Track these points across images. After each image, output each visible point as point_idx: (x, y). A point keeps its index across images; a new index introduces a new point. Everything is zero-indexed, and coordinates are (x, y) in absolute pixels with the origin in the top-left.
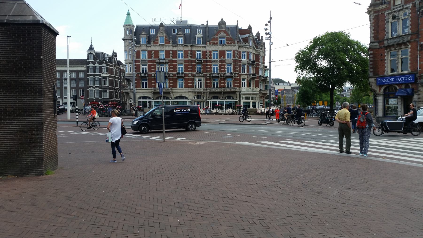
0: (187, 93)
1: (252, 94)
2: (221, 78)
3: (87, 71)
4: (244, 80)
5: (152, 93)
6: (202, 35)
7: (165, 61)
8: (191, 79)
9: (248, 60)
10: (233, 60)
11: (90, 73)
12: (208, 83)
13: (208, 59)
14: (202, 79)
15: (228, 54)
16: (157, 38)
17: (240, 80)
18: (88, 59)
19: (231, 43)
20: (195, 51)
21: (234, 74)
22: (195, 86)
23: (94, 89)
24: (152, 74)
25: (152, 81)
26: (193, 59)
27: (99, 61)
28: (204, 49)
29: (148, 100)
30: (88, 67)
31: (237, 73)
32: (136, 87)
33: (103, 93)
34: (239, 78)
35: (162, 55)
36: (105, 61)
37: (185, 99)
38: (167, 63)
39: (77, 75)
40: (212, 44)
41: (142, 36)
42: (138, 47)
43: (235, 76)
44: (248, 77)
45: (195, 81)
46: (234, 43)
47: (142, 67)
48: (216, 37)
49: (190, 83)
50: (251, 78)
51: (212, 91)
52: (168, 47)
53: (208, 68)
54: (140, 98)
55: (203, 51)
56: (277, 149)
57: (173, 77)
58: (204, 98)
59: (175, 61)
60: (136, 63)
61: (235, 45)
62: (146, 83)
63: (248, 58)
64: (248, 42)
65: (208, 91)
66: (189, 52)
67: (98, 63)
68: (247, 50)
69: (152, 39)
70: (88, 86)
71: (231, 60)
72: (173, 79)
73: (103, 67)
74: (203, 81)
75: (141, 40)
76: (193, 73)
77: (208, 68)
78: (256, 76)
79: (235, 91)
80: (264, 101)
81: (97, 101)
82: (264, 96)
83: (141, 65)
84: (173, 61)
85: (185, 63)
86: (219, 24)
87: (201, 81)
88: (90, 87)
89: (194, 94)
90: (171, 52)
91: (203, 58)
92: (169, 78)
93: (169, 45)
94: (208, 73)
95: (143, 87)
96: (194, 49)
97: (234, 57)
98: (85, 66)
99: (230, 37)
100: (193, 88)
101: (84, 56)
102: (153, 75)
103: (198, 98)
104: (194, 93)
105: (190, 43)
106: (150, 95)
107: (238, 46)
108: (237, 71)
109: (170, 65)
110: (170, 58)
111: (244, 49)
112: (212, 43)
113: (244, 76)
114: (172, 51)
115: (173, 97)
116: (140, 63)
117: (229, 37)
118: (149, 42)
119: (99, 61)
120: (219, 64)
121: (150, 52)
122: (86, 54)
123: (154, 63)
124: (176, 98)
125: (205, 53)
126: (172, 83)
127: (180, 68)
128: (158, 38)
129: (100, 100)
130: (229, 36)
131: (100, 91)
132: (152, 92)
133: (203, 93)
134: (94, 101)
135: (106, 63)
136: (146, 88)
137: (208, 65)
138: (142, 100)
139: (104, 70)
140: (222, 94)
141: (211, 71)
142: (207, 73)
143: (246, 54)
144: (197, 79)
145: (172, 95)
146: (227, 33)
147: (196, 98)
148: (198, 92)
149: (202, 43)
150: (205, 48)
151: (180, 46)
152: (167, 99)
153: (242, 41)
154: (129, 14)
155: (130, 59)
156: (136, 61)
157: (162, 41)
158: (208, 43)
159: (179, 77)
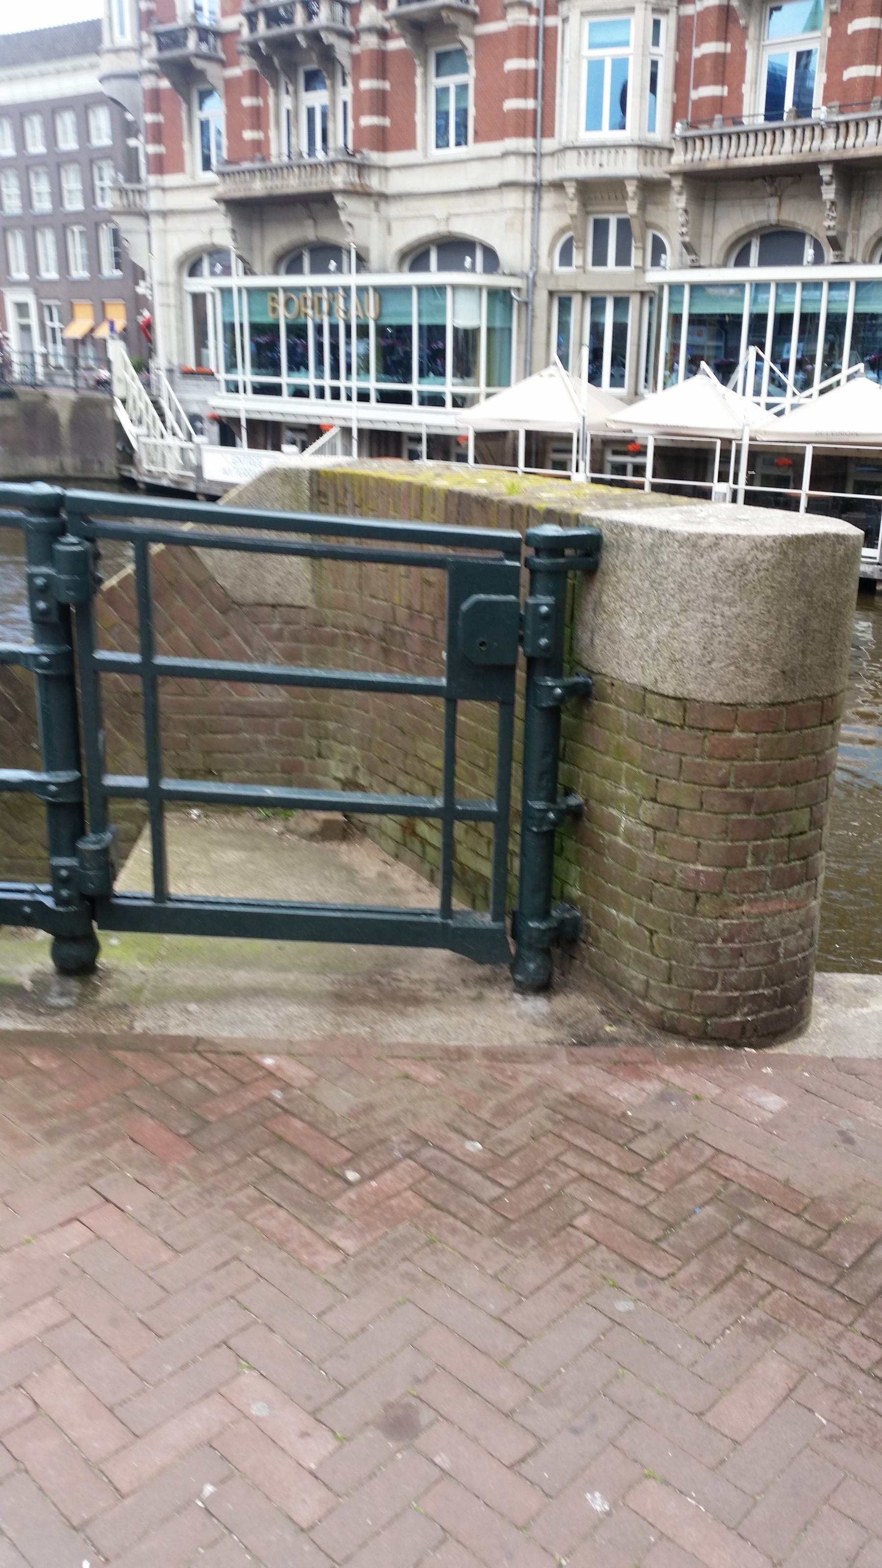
0: (493, 201)
56: (357, 919)
87: (626, 44)
95: (442, 141)
100: (548, 144)
103: (600, 259)
136: (462, 152)
140: (829, 193)
147: (582, 257)
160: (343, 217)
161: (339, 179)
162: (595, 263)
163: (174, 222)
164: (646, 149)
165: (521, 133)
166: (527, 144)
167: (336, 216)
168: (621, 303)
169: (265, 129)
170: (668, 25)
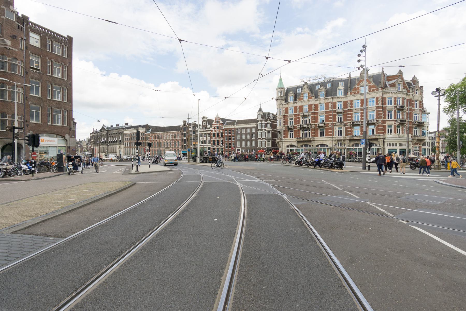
0: (328, 141)
1: (400, 141)
2: (378, 124)
3: (257, 127)
4: (390, 126)
5: (296, 141)
6: (343, 87)
7: (307, 114)
8: (331, 128)
9: (395, 106)
10: (376, 107)
11: (259, 129)
12: (348, 131)
13: (349, 108)
14: (343, 128)
15: (389, 101)
16: (301, 95)
17: (385, 127)
18: (258, 118)
19: (373, 90)
20: (336, 103)
21: (377, 121)
22: (335, 135)
23: (261, 141)
24: (297, 126)
25: (297, 132)
26: (333, 110)
27: (265, 119)
28: (345, 100)
29: (294, 148)
30: (257, 125)
31: (380, 119)
32: (284, 137)
33: (267, 143)
34: (383, 124)
35: (306, 108)
36: (269, 118)
37: (326, 147)
38: (309, 115)
39: (251, 131)
40: (353, 94)
41: (290, 95)
42: (286, 105)
43: (378, 123)
44: (395, 123)
45: (335, 130)
46: (377, 90)
47: (289, 121)
48: (358, 86)
49: (331, 132)
50: (398, 123)
51: (352, 139)
52: (310, 102)
53: (348, 117)
54: (288, 147)
55: (344, 102)
57: (315, 127)
58: (344, 146)
59: (317, 113)
60: (285, 118)
61: (379, 92)
62: (323, 132)
63: (395, 104)
64: (395, 87)
65: (348, 138)
66: (330, 104)
67: (264, 120)
68: (394, 95)
69: (298, 97)
70: (257, 138)
71: (374, 107)
72: (314, 130)
73: (267, 123)
74: (343, 129)
75: (289, 99)
76: (333, 123)
77: (348, 117)
78: (406, 122)
79: (378, 138)
80: (420, 147)
81: (263, 149)
82: (420, 143)
83: (289, 119)
84: (315, 113)
85: (326, 114)
86: (360, 74)
88: (259, 139)
89: (334, 142)
90: (313, 106)
91: (344, 108)
92: (312, 128)
93: (312, 99)
94: (349, 122)
96: (335, 100)
97: (377, 104)
98: (255, 124)
99: (373, 84)
100: (333, 137)
101: (255, 116)
102: (349, 124)
103: (338, 146)
104: (335, 141)
105: (331, 96)
106: (295, 144)
107: (381, 93)
108: (381, 118)
109: (312, 117)
110: (312, 111)
111: (390, 95)
112: (353, 93)
113: (391, 122)
114: (315, 104)
115: (315, 145)
116: (287, 118)
117: (371, 84)
118: (295, 100)
119: (265, 119)
120: (375, 111)
121: (295, 108)
122: (257, 114)
123: (299, 117)
124: (317, 146)
125: (345, 104)
126: (314, 133)
127: (321, 118)
128: (303, 95)
129: (265, 149)
130: (372, 83)
131: (266, 142)
132: (296, 141)
133: (343, 140)
134: (261, 149)
135: (270, 120)
136: (292, 138)
137: (348, 114)
138: (289, 148)
139: (269, 125)
141: (352, 119)
142: (348, 122)
143: (393, 99)
144: (337, 128)
145: (314, 143)
146: (370, 81)
148: (338, 140)
149: (343, 94)
150: (346, 99)
151: (321, 100)
152: (309, 147)
153: (388, 86)
154: (281, 80)
155: (280, 115)
156: (284, 116)
157: (305, 97)
158: (349, 93)
159: (354, 125)
160: (379, 141)
161: (312, 139)
162: (338, 146)
163: (286, 142)
164: (344, 137)
165: (331, 136)
166: (332, 137)
167: (378, 140)
168: (344, 149)
169: (300, 134)
170: (345, 128)
